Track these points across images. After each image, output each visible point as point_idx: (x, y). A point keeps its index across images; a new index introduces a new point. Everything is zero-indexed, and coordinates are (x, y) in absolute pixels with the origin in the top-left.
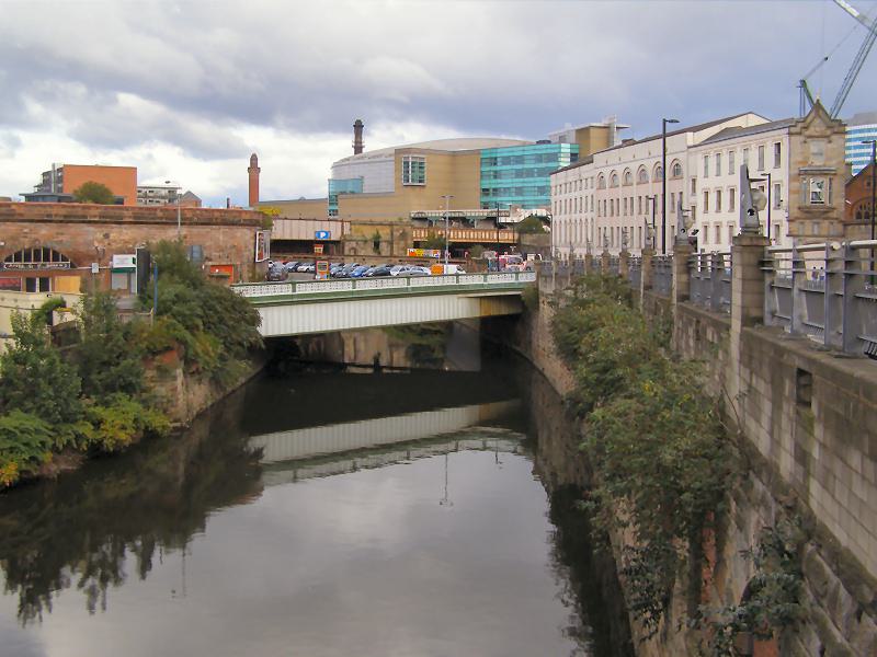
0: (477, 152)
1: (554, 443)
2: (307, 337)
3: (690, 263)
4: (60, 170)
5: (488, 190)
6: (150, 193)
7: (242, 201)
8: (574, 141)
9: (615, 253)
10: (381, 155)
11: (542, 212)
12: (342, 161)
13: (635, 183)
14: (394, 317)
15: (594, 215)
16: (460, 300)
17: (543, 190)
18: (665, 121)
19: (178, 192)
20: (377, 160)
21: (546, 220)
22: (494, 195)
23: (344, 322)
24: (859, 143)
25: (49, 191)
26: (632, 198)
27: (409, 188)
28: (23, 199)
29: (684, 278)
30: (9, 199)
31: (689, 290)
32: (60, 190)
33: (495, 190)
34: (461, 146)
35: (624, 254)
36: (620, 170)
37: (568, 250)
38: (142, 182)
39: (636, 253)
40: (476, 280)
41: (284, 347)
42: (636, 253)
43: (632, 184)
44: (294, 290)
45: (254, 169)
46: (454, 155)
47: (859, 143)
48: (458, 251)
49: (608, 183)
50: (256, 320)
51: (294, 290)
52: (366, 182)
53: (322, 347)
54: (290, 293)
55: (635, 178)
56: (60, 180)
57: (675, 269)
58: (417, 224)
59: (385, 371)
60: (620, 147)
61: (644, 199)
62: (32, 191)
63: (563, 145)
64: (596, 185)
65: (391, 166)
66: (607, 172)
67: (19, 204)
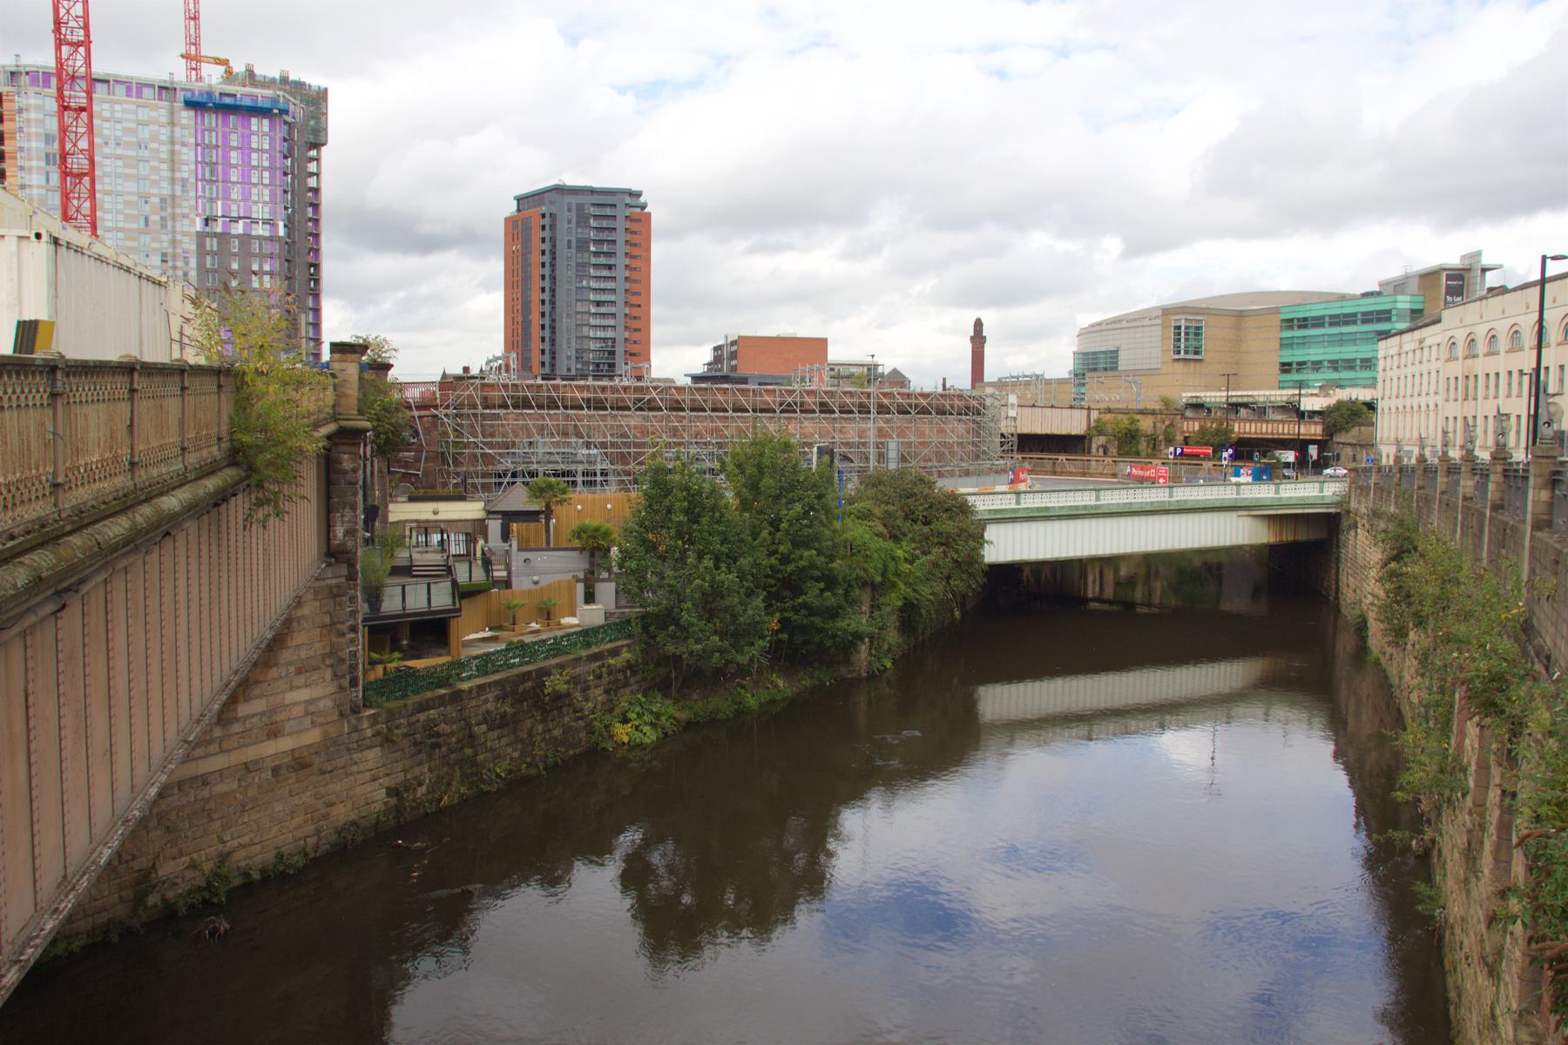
0: (1276, 311)
1: (1364, 718)
2: (1038, 566)
3: (1559, 473)
4: (734, 343)
5: (1290, 364)
6: (840, 374)
7: (961, 379)
8: (1416, 292)
9: (1455, 454)
10: (1120, 321)
11: (1364, 395)
12: (1092, 326)
13: (1481, 355)
14: (1228, 537)
15: (1440, 399)
16: (1241, 519)
17: (1368, 364)
18: (1544, 258)
19: (880, 370)
20: (1118, 326)
21: (1371, 406)
22: (1298, 370)
23: (1231, 538)
24: (267, 582)
25: (721, 370)
26: (1497, 374)
27: (1181, 364)
28: (688, 381)
29: (1544, 495)
30: (672, 381)
31: (1550, 513)
32: (734, 368)
33: (1299, 364)
34: (1252, 303)
35: (1469, 457)
36: (1481, 332)
37: (1392, 450)
38: (835, 354)
39: (1484, 456)
40: (1265, 492)
41: (1009, 572)
42: (1484, 456)
43: (1457, 359)
44: (1018, 502)
45: (978, 339)
46: (1240, 315)
47: (267, 582)
48: (1245, 450)
49: (1481, 347)
50: (978, 538)
51: (1018, 502)
52: (1122, 356)
53: (1058, 575)
54: (1093, 503)
55: (1503, 343)
56: (733, 355)
57: (1531, 480)
58: (1189, 413)
59: (1094, 605)
60: (1481, 299)
61: (1515, 375)
62: (700, 369)
63: (1400, 298)
64: (1444, 353)
65: (1158, 331)
66: (1460, 336)
67: (680, 389)
